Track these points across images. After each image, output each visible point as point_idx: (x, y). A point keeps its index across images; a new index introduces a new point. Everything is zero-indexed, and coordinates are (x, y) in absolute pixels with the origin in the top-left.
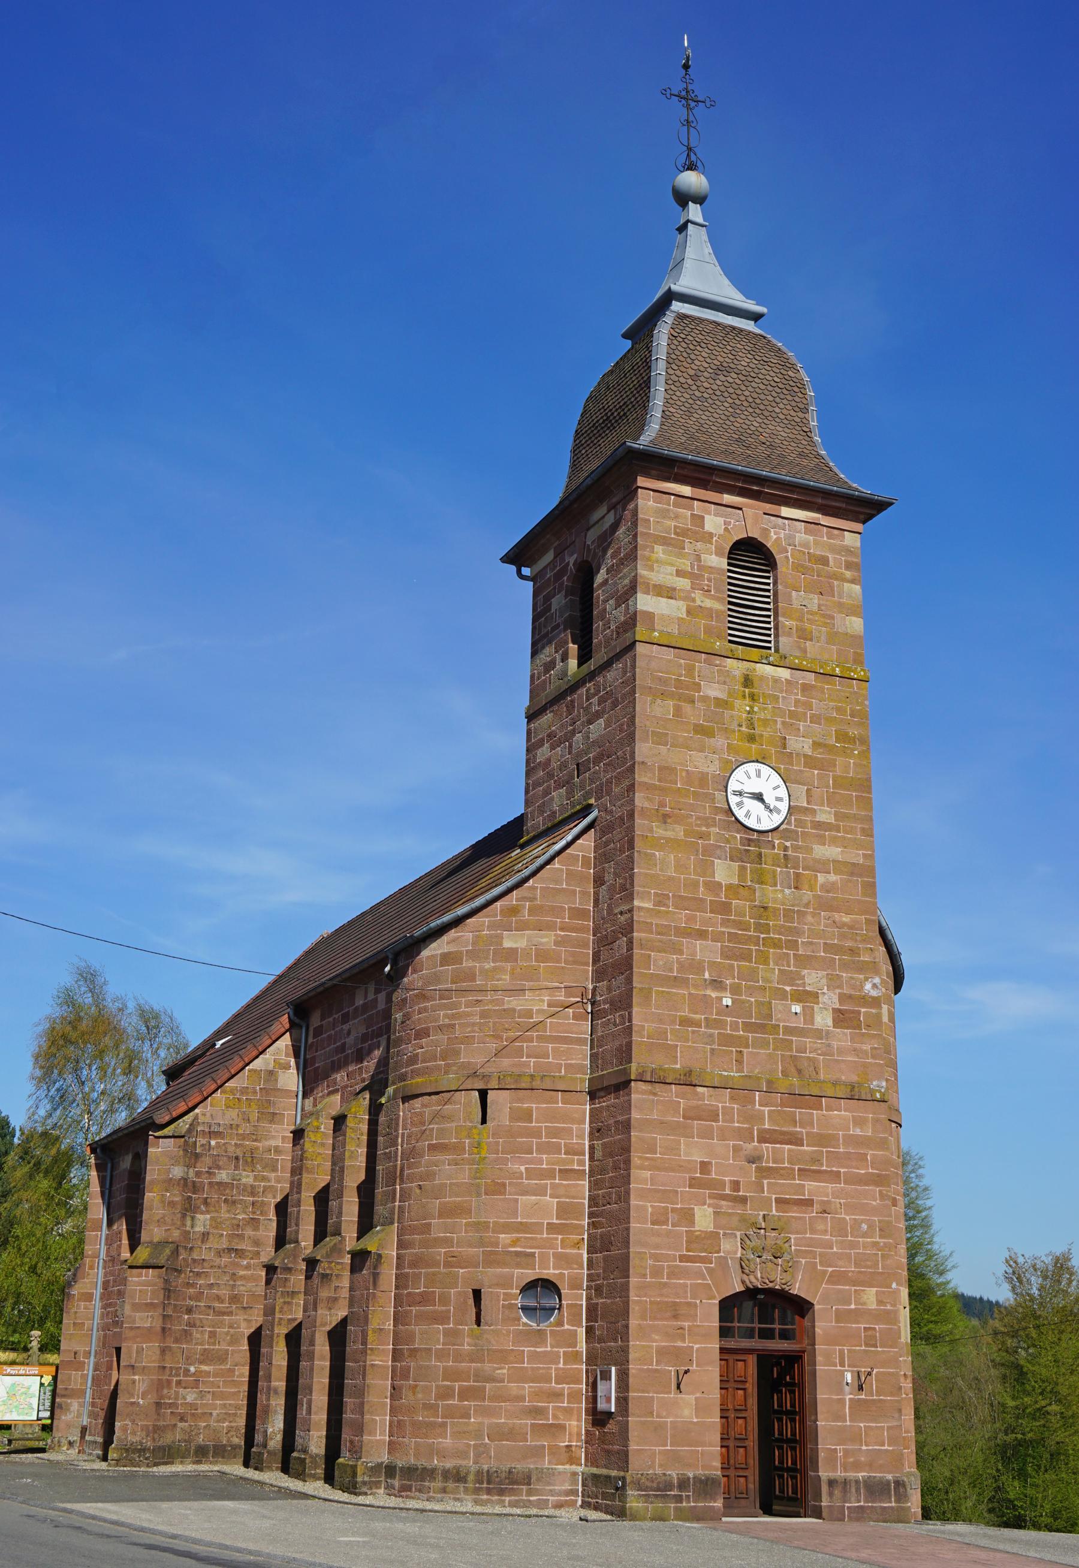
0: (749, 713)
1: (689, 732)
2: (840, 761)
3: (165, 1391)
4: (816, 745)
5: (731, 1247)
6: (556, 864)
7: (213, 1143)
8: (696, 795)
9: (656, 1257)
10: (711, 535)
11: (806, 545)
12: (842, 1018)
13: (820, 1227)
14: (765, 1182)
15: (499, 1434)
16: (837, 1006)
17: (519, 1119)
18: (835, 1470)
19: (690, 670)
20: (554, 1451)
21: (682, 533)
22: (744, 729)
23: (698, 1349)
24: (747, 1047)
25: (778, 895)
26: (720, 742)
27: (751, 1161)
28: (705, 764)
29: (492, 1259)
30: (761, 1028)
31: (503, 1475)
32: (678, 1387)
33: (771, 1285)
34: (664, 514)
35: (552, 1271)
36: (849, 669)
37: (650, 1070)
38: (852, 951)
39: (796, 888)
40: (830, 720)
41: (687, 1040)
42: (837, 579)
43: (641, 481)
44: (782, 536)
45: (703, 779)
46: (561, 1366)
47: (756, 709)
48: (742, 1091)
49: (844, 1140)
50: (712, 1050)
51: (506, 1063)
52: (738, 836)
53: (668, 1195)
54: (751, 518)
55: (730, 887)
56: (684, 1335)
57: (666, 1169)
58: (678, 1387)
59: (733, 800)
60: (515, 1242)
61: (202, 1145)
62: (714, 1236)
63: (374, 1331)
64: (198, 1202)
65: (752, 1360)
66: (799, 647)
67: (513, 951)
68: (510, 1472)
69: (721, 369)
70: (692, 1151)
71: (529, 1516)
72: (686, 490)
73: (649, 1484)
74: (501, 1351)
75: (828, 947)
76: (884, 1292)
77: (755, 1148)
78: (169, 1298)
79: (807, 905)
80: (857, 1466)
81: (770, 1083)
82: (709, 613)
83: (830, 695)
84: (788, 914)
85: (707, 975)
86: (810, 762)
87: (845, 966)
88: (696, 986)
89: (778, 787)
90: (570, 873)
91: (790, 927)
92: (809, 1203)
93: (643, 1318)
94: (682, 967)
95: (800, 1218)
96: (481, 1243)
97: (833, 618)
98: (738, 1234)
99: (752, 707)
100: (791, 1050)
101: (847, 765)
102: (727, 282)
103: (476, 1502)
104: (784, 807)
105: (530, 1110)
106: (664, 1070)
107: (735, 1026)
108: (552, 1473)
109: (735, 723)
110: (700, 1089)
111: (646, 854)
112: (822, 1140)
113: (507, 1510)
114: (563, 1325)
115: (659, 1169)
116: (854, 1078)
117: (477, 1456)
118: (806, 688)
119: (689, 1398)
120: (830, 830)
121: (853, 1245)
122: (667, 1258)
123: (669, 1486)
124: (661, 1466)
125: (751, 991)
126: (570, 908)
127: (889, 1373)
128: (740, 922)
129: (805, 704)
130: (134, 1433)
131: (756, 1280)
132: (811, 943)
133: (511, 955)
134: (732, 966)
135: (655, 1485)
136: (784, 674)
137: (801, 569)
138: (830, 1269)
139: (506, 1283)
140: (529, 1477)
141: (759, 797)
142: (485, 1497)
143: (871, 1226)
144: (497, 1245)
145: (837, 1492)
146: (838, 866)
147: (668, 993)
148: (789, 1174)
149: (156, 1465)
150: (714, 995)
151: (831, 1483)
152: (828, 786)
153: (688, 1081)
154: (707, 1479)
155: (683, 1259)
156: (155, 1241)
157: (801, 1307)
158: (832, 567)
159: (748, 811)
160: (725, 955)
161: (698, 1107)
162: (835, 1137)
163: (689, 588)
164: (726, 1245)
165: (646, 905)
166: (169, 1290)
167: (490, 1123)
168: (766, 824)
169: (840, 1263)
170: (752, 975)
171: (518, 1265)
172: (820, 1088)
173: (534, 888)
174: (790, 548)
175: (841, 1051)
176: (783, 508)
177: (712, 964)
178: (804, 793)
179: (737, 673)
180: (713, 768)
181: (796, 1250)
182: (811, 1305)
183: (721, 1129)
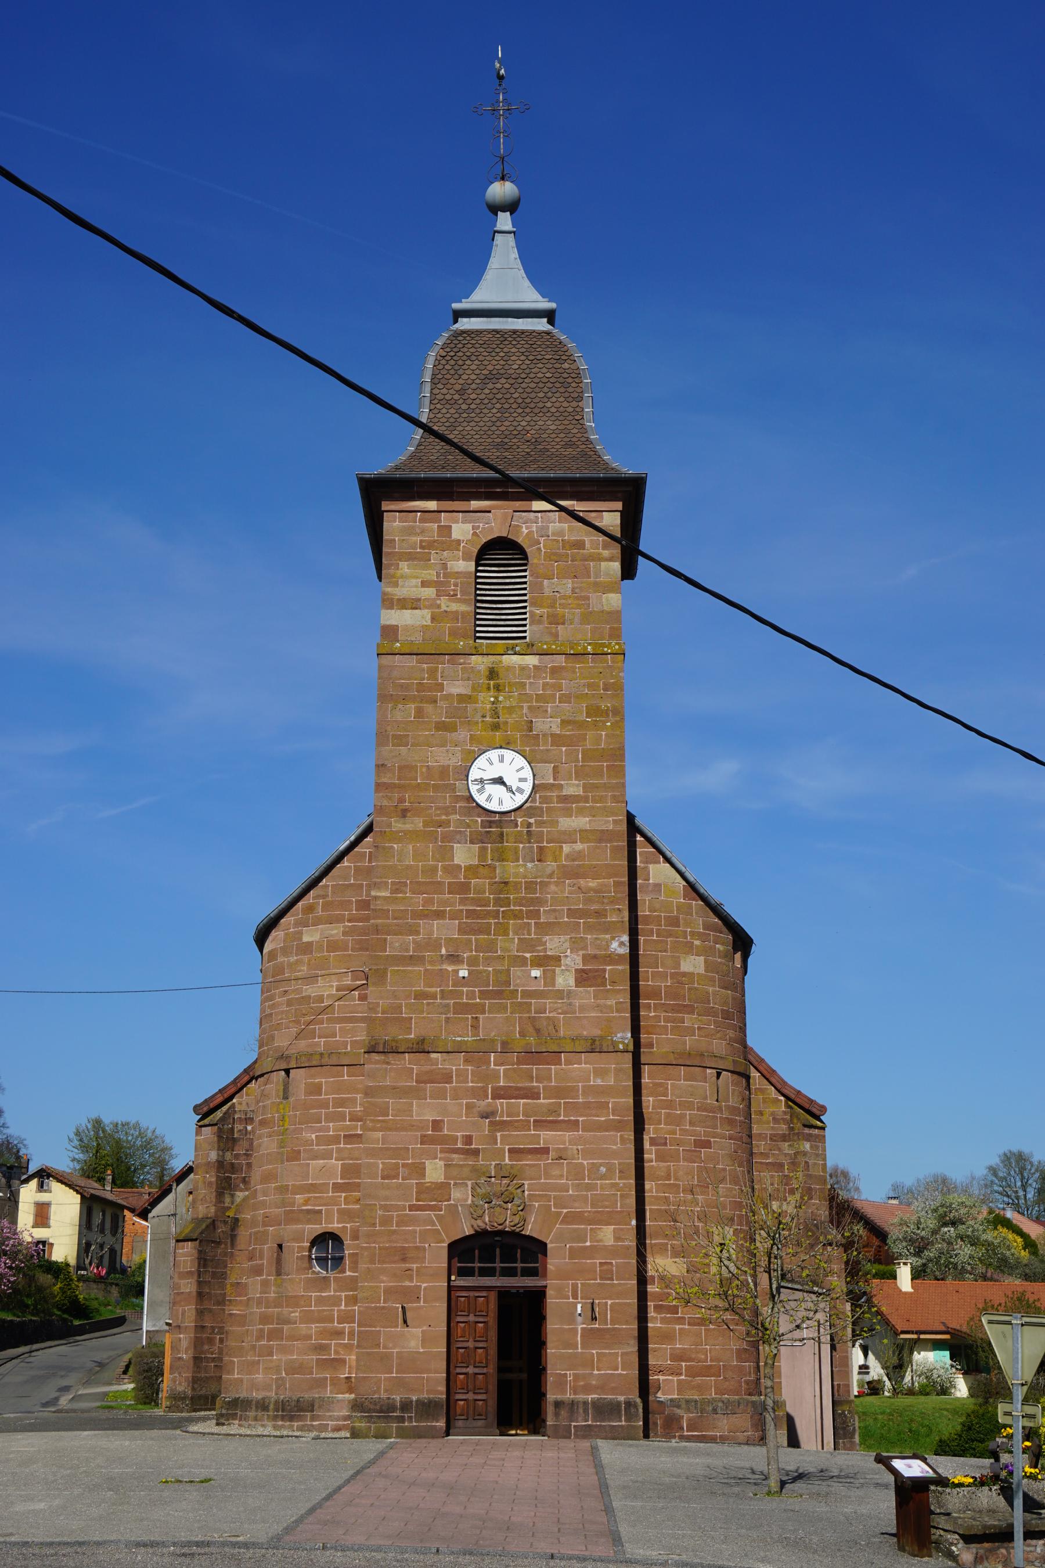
0: (493, 703)
1: (430, 730)
2: (590, 734)
3: (206, 1347)
4: (564, 723)
5: (462, 1195)
6: (345, 863)
7: (249, 1128)
8: (436, 788)
9: (385, 1208)
10: (458, 542)
11: (561, 533)
12: (583, 978)
13: (556, 1172)
14: (499, 1134)
15: (294, 1369)
16: (581, 967)
17: (311, 1093)
18: (564, 1392)
19: (433, 672)
20: (335, 1381)
21: (430, 545)
22: (488, 719)
23: (425, 1288)
24: (483, 1012)
25: (520, 869)
26: (463, 734)
27: (485, 1116)
28: (445, 757)
29: (291, 1217)
30: (499, 994)
31: (293, 1404)
32: (405, 1322)
33: (500, 1227)
34: (410, 531)
35: (336, 1225)
36: (603, 645)
37: (382, 1042)
38: (599, 914)
39: (539, 861)
40: (580, 697)
41: (423, 1012)
42: (593, 560)
43: (386, 506)
44: (534, 529)
45: (444, 771)
46: (343, 1307)
47: (501, 698)
48: (475, 1053)
49: (583, 1091)
50: (447, 1019)
51: (302, 1045)
52: (479, 820)
53: (399, 1152)
54: (494, 518)
55: (469, 868)
56: (412, 1276)
57: (397, 1129)
58: (405, 1322)
59: (474, 789)
60: (307, 1202)
61: (240, 1131)
62: (444, 1187)
63: (232, 1285)
64: (238, 1181)
65: (493, 1296)
66: (551, 633)
67: (310, 944)
68: (298, 1401)
69: (493, 377)
70: (424, 1111)
71: (282, 1437)
72: (432, 505)
73: (372, 1407)
74: (295, 1297)
75: (571, 913)
76: (622, 1229)
77: (489, 1104)
78: (205, 1266)
79: (551, 876)
80: (588, 1389)
81: (504, 1044)
82: (455, 616)
83: (581, 673)
84: (530, 886)
85: (444, 951)
86: (557, 740)
87: (589, 928)
88: (432, 963)
89: (523, 768)
90: (357, 870)
91: (532, 898)
92: (545, 1151)
93: (372, 1262)
94: (418, 946)
95: (534, 1165)
96: (283, 1204)
97: (588, 598)
98: (469, 1183)
99: (496, 698)
100: (529, 1011)
101: (601, 738)
102: (527, 283)
103: (275, 1427)
104: (528, 787)
105: (321, 1084)
106: (397, 1041)
107: (471, 995)
108: (331, 1401)
109: (479, 714)
110: (433, 1055)
111: (384, 848)
112: (559, 1092)
113: (331, 1435)
114: (345, 1272)
115: (390, 1130)
116: (597, 1032)
117: (278, 1388)
118: (555, 671)
119: (416, 1332)
120: (578, 802)
121: (589, 1187)
122: (397, 1208)
123: (392, 1408)
124: (386, 1391)
125: (488, 961)
126: (357, 901)
127: (625, 1304)
128: (479, 899)
129: (553, 686)
130: (180, 1384)
131: (486, 1222)
132: (554, 910)
133: (307, 948)
134: (470, 940)
135: (378, 1407)
136: (532, 660)
137: (553, 557)
138: (565, 1211)
139: (298, 1238)
140: (313, 1406)
141: (500, 781)
142: (280, 1423)
143: (610, 1169)
144: (293, 1204)
145: (563, 1413)
146: (584, 835)
147: (404, 971)
148: (525, 1125)
149: (195, 1411)
150: (450, 969)
151: (558, 1404)
152: (578, 761)
153: (421, 1048)
154: (430, 1401)
155: (412, 1208)
156: (200, 1216)
157: (535, 1249)
158: (589, 549)
159: (490, 795)
160: (461, 930)
161: (432, 1071)
162: (575, 1089)
163: (434, 596)
164: (456, 1194)
165: (383, 894)
166: (205, 1260)
167: (292, 1099)
168: (509, 805)
169: (576, 1205)
170: (491, 946)
171: (309, 1222)
172: (559, 1044)
173: (327, 886)
174: (542, 540)
175: (582, 1008)
176: (534, 503)
177: (449, 941)
178: (551, 770)
179: (482, 668)
180: (454, 760)
181: (529, 1195)
182: (542, 1247)
183: (455, 1089)
